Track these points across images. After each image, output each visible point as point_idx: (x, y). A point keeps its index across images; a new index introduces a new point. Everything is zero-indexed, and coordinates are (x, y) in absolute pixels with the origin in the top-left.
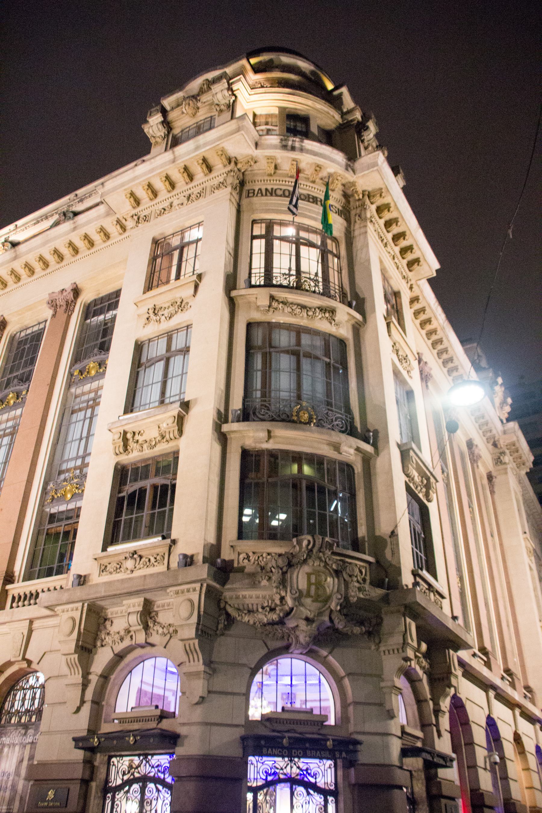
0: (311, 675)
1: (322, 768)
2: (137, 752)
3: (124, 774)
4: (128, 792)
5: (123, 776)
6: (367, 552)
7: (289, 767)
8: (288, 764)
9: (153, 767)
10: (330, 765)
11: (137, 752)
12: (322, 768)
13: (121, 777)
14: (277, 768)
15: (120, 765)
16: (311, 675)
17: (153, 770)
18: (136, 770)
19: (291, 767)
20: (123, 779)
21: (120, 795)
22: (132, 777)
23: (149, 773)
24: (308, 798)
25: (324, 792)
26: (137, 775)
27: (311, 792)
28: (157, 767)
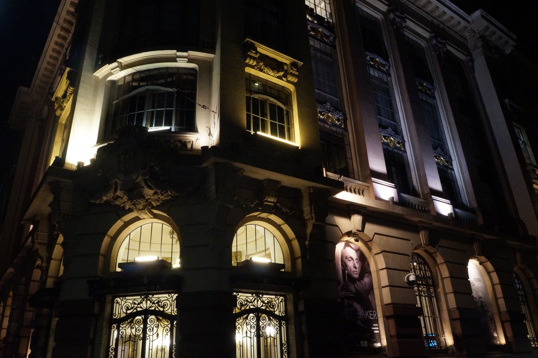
0: (133, 250)
1: (277, 301)
2: (253, 291)
3: (128, 309)
4: (247, 318)
5: (127, 310)
6: (356, 177)
7: (256, 301)
8: (255, 299)
9: (154, 303)
10: (282, 299)
11: (253, 291)
12: (277, 301)
13: (125, 311)
14: (248, 302)
15: (123, 303)
16: (133, 250)
17: (154, 305)
18: (139, 306)
19: (258, 301)
20: (126, 313)
21: (241, 321)
22: (135, 311)
23: (151, 307)
24: (157, 323)
25: (278, 318)
26: (139, 309)
27: (161, 318)
28: (157, 303)
